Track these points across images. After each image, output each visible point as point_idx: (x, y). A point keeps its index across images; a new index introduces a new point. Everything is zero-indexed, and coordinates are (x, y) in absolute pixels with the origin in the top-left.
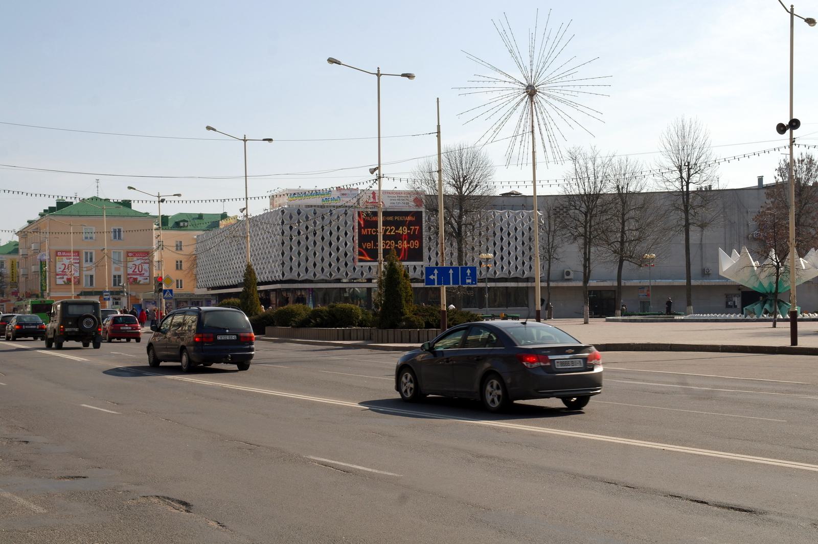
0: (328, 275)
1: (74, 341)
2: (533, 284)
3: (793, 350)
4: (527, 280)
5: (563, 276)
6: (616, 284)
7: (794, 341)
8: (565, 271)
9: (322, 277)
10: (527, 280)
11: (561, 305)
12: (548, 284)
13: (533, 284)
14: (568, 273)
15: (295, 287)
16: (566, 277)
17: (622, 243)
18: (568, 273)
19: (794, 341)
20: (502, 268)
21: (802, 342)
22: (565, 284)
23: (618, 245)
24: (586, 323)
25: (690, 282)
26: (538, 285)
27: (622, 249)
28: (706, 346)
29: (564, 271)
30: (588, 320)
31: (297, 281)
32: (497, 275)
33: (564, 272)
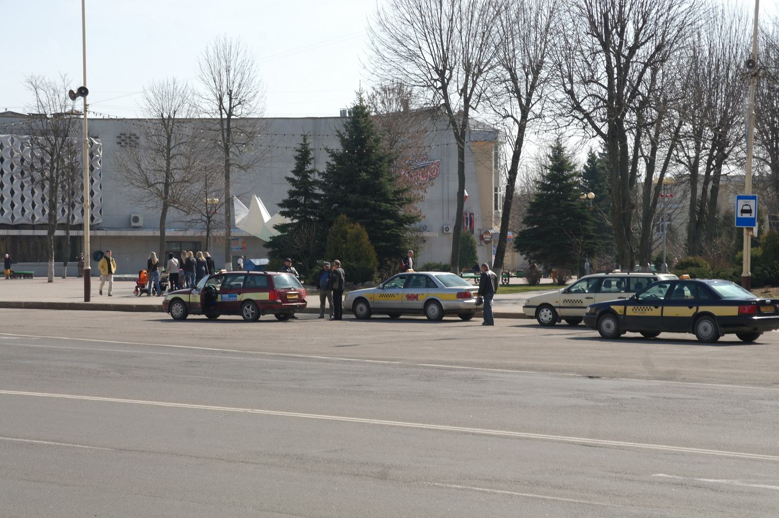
0: (10, 218)
1: (765, 333)
2: (81, 233)
3: (86, 306)
4: (76, 227)
5: (130, 223)
6: (158, 233)
7: (87, 296)
8: (133, 216)
9: (24, 221)
10: (76, 227)
11: (127, 259)
12: (163, 232)
13: (81, 233)
14: (136, 219)
15: (40, 234)
16: (133, 224)
17: (167, 185)
18: (136, 219)
19: (87, 296)
20: (23, 210)
21: (95, 300)
22: (130, 233)
23: (161, 187)
24: (50, 281)
25: (230, 232)
26: (87, 233)
27: (166, 192)
28: (11, 303)
29: (131, 216)
30: (52, 278)
31: (10, 225)
32: (36, 220)
33: (130, 219)
